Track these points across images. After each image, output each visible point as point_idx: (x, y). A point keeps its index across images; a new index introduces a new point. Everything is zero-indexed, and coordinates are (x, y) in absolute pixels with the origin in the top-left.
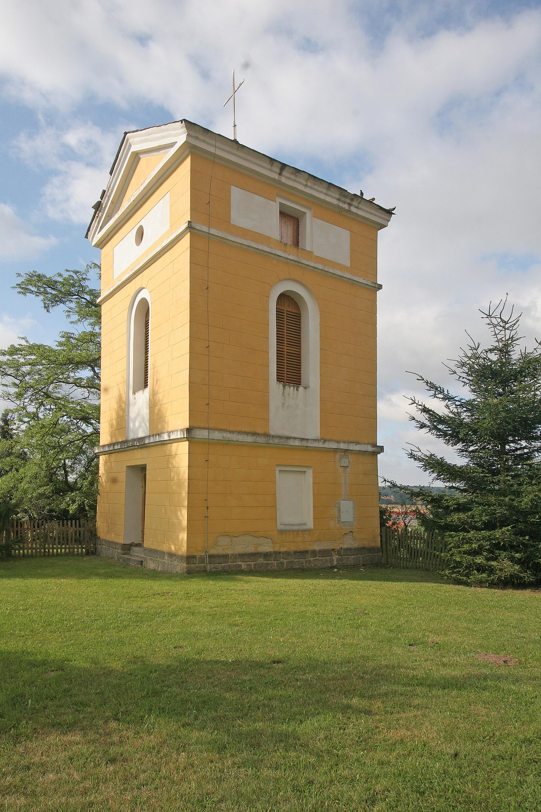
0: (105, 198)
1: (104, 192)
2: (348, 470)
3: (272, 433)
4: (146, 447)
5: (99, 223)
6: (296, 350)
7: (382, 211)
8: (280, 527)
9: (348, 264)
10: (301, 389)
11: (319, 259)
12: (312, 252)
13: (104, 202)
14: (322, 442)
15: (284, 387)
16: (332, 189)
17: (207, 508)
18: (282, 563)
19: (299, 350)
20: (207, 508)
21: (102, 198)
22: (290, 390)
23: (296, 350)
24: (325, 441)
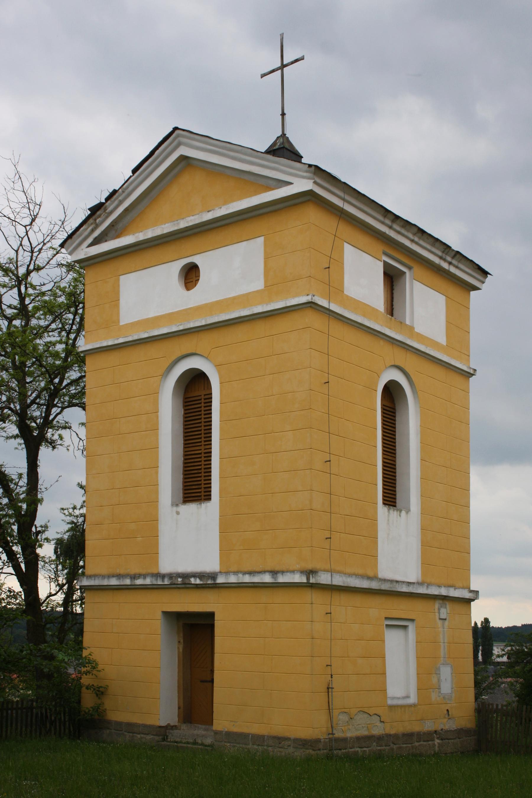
0: (115, 200)
1: (115, 192)
2: (447, 623)
3: (381, 575)
4: (219, 587)
5: (93, 231)
6: (389, 458)
7: (479, 272)
8: (390, 702)
9: (442, 340)
10: (403, 513)
11: (421, 338)
12: (413, 328)
13: (110, 206)
14: (425, 587)
15: (389, 510)
16: (437, 244)
17: (332, 676)
18: (392, 749)
19: (393, 459)
20: (332, 676)
21: (107, 199)
22: (394, 514)
23: (389, 458)
24: (429, 585)
